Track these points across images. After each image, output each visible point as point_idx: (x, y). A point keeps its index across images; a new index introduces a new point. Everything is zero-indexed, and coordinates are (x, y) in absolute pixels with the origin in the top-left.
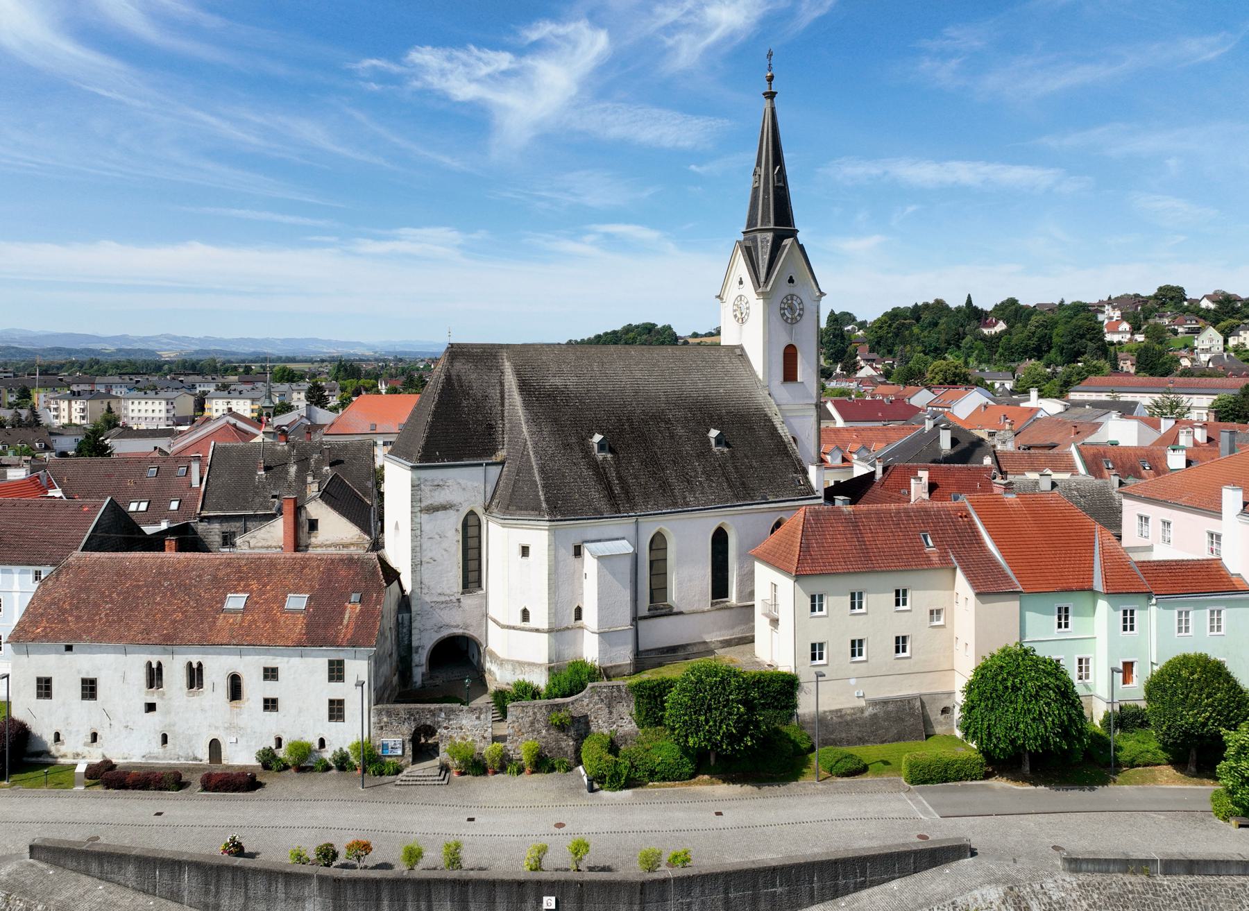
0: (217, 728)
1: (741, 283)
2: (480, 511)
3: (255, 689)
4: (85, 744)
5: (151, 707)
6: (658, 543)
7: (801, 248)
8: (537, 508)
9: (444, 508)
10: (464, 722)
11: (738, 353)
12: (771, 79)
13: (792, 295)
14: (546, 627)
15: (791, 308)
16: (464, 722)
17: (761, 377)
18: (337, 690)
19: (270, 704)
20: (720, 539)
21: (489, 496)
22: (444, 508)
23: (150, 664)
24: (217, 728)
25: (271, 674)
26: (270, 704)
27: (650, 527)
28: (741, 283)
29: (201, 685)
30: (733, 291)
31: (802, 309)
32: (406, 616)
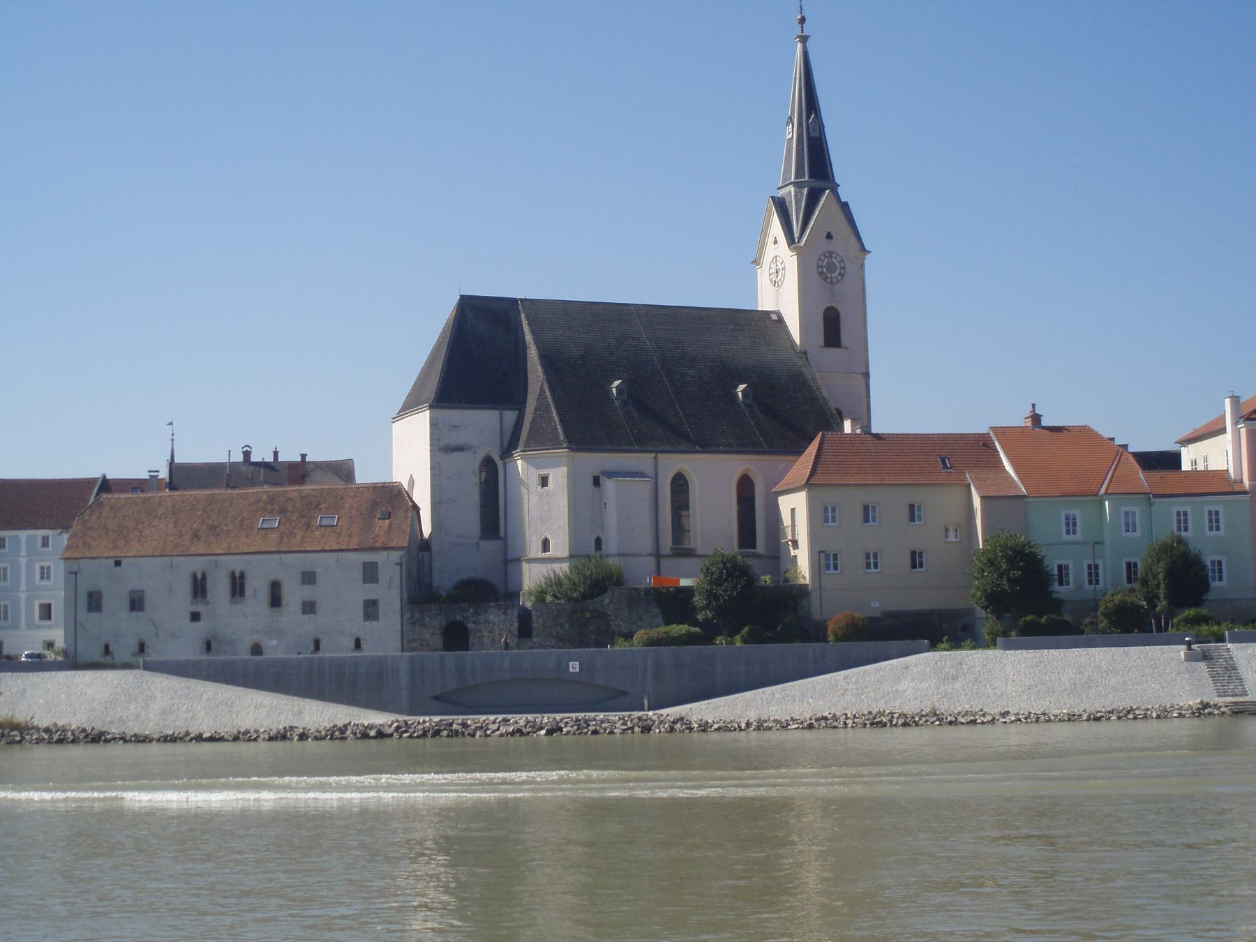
0: (258, 632)
1: (776, 242)
2: (496, 458)
3: (293, 594)
4: (134, 654)
5: (195, 617)
6: (680, 484)
7: (845, 207)
8: (557, 445)
9: (459, 449)
10: (492, 617)
11: (773, 322)
12: (802, 20)
13: (831, 253)
14: (566, 554)
15: (831, 267)
16: (492, 617)
17: (797, 341)
18: (371, 591)
19: (309, 607)
20: (745, 487)
21: (506, 444)
22: (459, 449)
23: (195, 575)
24: (258, 632)
25: (309, 578)
26: (309, 607)
27: (672, 463)
28: (776, 242)
29: (242, 594)
30: (770, 251)
31: (844, 268)
32: (426, 554)
